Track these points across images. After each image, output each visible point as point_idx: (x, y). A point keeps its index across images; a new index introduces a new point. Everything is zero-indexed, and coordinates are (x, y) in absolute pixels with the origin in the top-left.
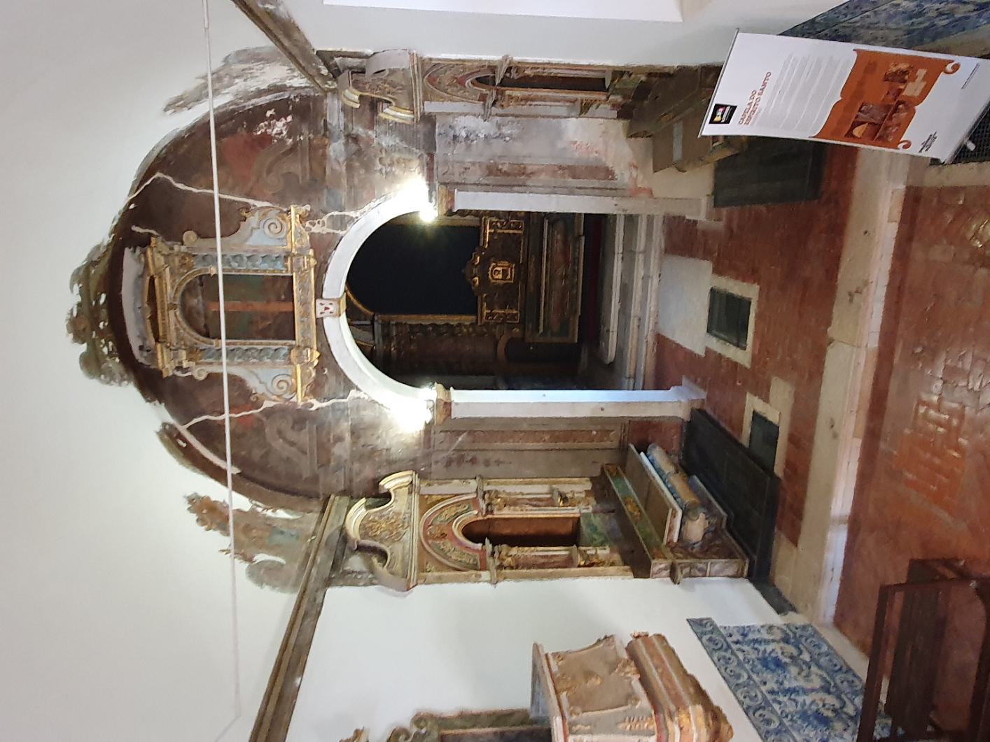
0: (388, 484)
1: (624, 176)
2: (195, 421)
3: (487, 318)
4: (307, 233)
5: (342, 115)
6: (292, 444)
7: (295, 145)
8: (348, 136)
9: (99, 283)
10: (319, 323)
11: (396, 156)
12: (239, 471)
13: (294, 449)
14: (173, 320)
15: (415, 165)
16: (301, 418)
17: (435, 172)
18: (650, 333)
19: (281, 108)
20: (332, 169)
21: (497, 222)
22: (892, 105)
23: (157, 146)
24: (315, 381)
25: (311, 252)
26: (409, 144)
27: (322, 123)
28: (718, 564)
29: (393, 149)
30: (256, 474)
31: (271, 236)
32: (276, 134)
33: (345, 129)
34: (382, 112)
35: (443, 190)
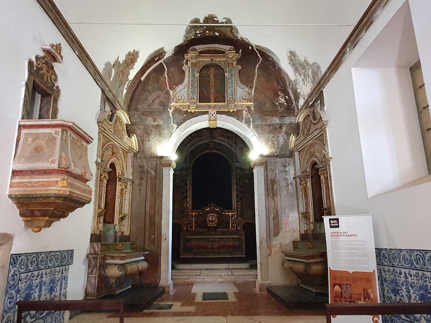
0: (134, 138)
1: (276, 241)
2: (165, 66)
3: (191, 215)
4: (243, 109)
5: (289, 122)
6: (153, 101)
7: (277, 106)
8: (281, 125)
9: (223, 33)
10: (207, 113)
11: (276, 143)
12: (142, 80)
13: (151, 102)
14: (206, 60)
15: (273, 150)
16: (165, 105)
17: (271, 158)
18: (194, 280)
19: (289, 101)
20: (268, 118)
21: (234, 217)
22: (352, 299)
23: (274, 54)
24: (181, 111)
25: (235, 110)
26: (281, 148)
27: (285, 115)
28: (94, 281)
29: (278, 142)
30: (140, 87)
31: (241, 96)
32: (279, 99)
33: (284, 124)
34: (293, 135)
35: (264, 161)
